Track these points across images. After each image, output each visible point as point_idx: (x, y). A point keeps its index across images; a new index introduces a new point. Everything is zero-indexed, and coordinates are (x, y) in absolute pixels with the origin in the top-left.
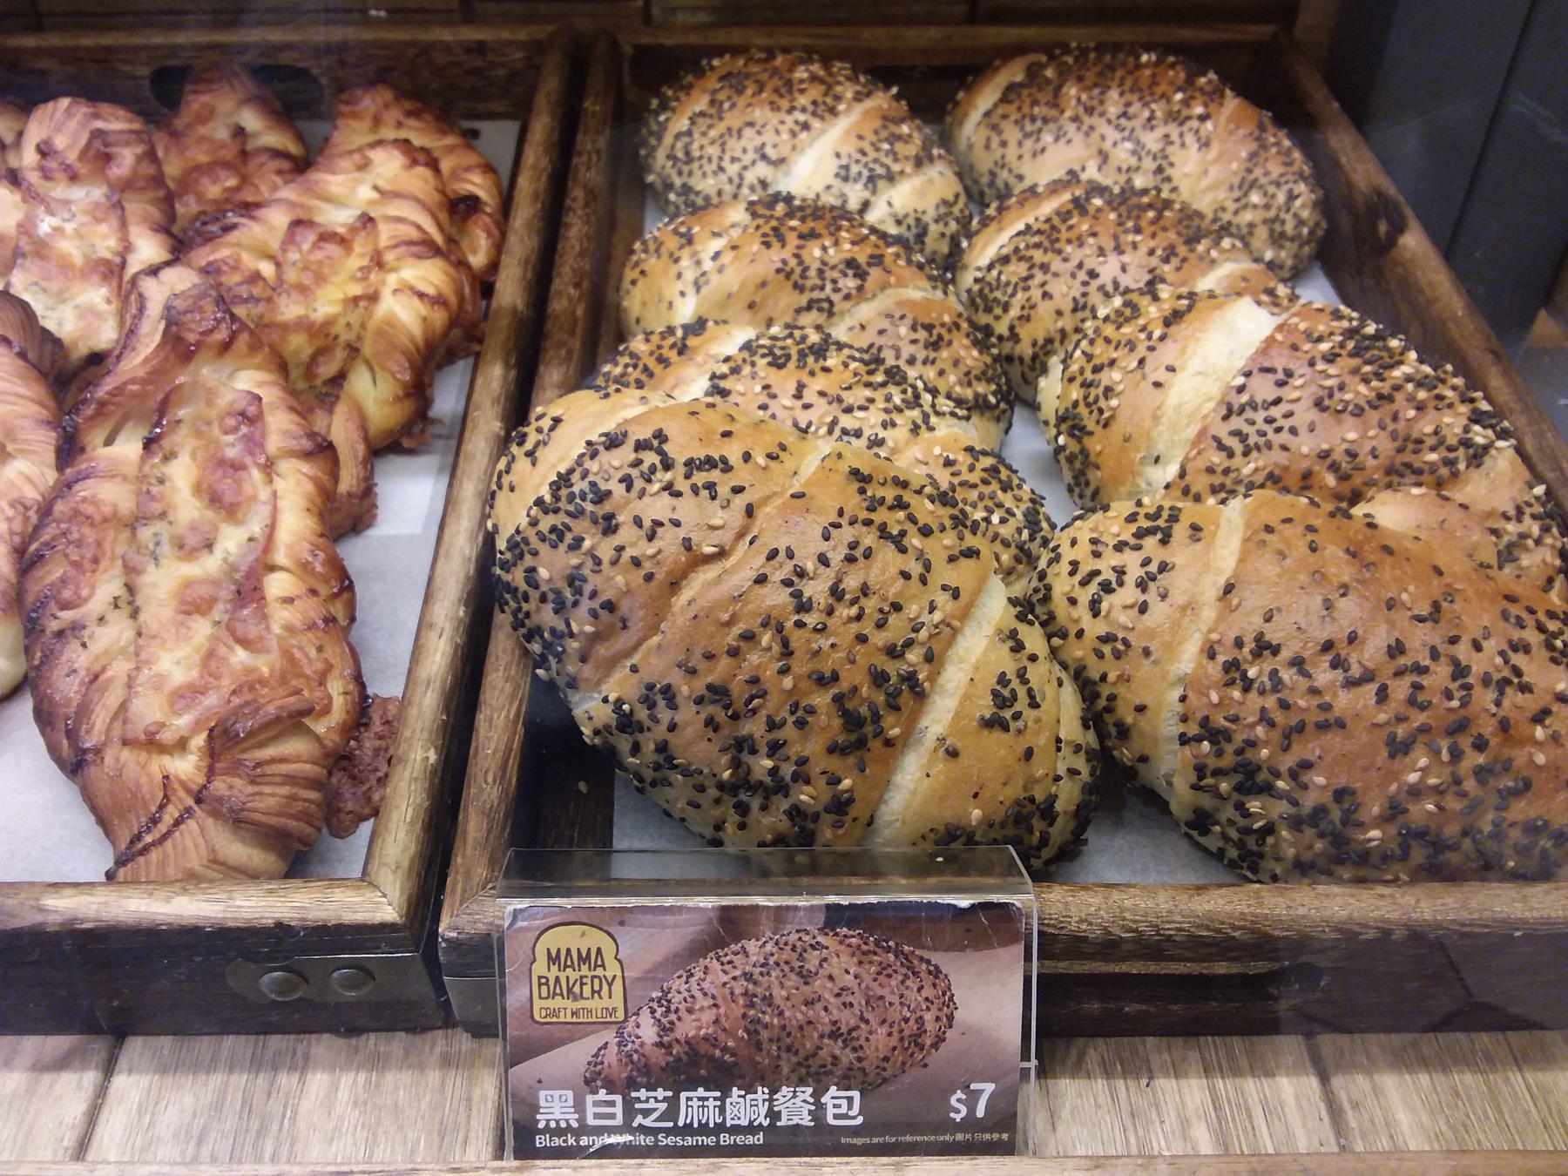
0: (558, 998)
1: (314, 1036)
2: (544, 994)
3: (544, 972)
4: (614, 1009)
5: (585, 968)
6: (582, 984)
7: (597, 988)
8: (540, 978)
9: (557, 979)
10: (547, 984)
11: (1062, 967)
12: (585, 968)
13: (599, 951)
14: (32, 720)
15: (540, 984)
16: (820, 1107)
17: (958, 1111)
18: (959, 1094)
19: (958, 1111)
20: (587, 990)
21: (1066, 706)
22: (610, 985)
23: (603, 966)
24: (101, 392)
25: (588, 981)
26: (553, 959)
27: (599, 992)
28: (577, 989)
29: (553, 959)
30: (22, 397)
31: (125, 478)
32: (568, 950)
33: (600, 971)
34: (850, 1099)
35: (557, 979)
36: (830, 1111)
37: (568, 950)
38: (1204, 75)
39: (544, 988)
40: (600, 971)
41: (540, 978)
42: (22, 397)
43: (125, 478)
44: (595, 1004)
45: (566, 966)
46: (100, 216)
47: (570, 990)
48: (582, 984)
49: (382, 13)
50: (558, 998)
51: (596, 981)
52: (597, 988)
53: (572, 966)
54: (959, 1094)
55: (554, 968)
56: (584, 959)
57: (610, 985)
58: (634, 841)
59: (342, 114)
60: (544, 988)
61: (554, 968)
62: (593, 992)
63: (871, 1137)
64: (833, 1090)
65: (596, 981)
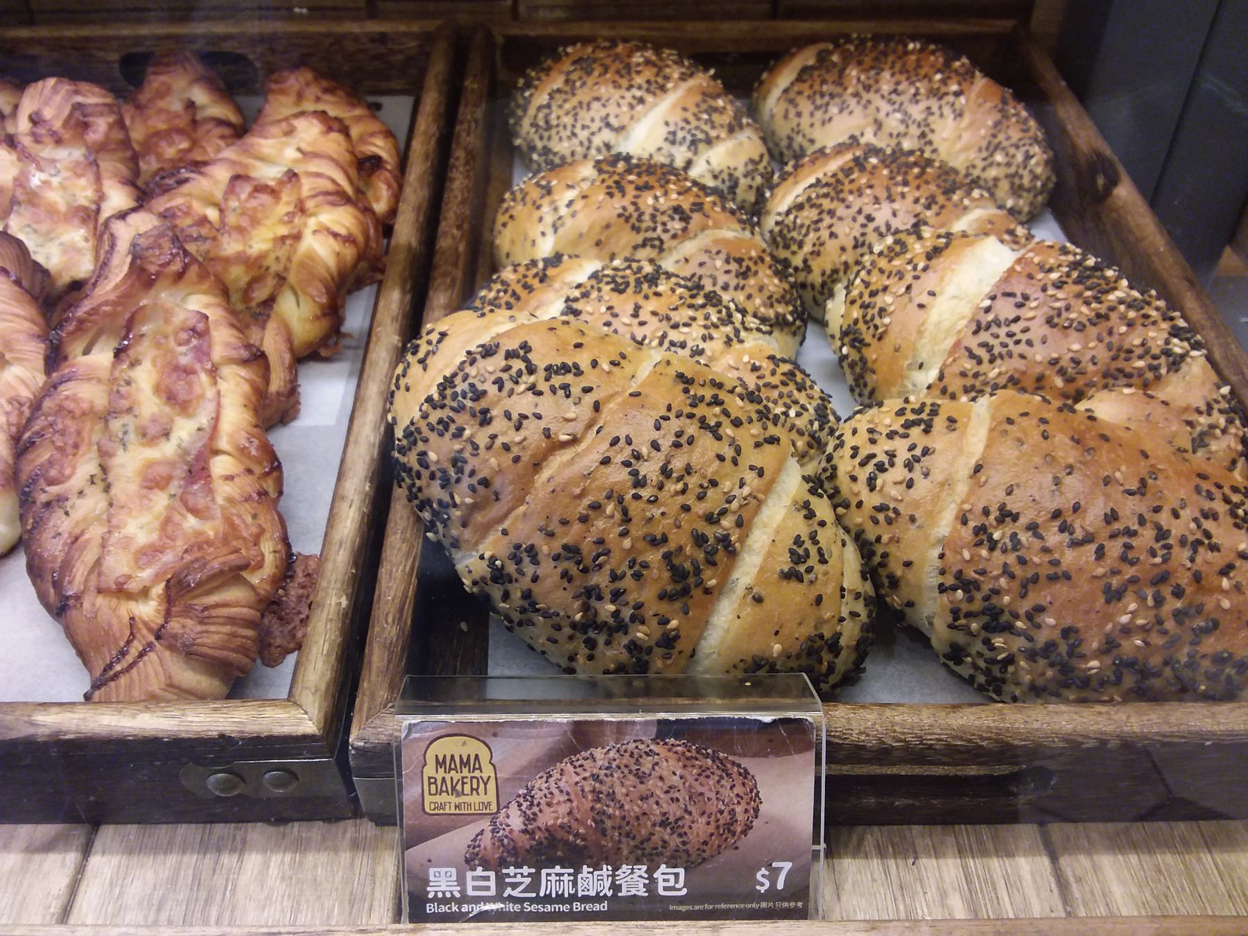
0: (444, 794)
1: (250, 825)
2: (433, 791)
3: (433, 774)
4: (489, 803)
5: (465, 770)
6: (463, 783)
7: (475, 786)
8: (430, 778)
9: (444, 779)
10: (435, 783)
11: (845, 769)
12: (465, 770)
13: (477, 757)
14: (26, 573)
15: (430, 784)
16: (652, 881)
17: (762, 884)
18: (764, 871)
19: (762, 884)
20: (467, 788)
21: (849, 562)
22: (485, 784)
23: (480, 769)
24: (81, 312)
25: (468, 780)
26: (440, 763)
27: (477, 790)
28: (459, 787)
29: (440, 763)
30: (17, 316)
31: (99, 381)
32: (452, 756)
33: (477, 773)
34: (677, 875)
35: (444, 779)
36: (661, 885)
37: (452, 756)
38: (958, 59)
39: (433, 787)
40: (477, 773)
41: (430, 778)
42: (17, 316)
43: (99, 381)
44: (474, 799)
45: (450, 769)
46: (79, 172)
47: (453, 788)
48: (463, 783)
49: (304, 11)
50: (444, 794)
51: (475, 781)
52: (475, 786)
53: (455, 769)
54: (764, 871)
55: (441, 771)
56: (465, 763)
57: (485, 784)
58: (505, 670)
59: (272, 91)
60: (433, 787)
61: (441, 771)
62: (472, 789)
63: (693, 905)
64: (663, 868)
65: (475, 781)
